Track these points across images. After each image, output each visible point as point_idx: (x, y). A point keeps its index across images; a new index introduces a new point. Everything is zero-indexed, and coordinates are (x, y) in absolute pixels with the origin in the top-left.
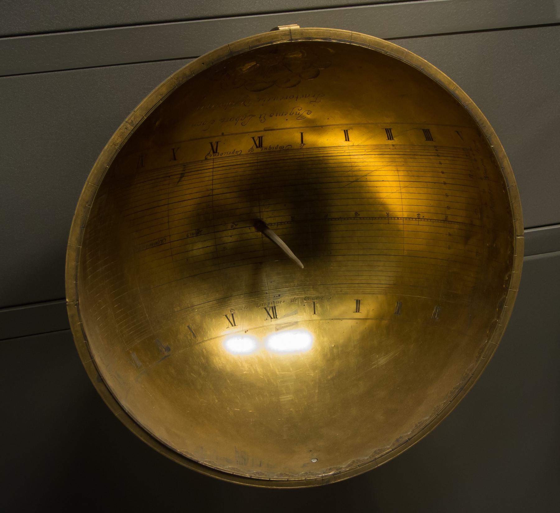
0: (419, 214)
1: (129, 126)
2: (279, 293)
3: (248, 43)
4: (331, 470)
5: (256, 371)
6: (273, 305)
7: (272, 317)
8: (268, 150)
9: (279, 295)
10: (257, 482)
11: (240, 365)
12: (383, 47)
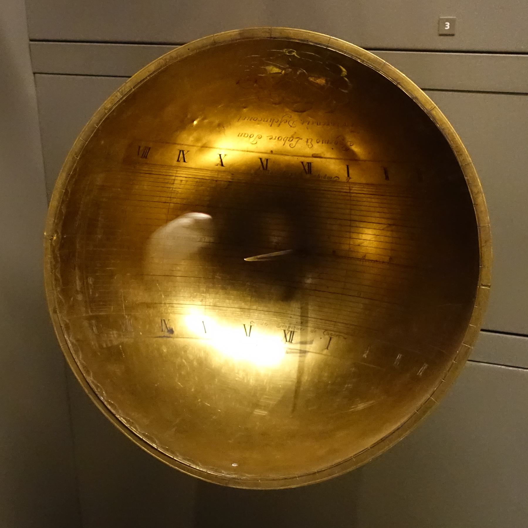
3: (231, 36)
5: (248, 381)
6: (293, 330)
7: (288, 340)
10: (163, 455)
12: (360, 56)
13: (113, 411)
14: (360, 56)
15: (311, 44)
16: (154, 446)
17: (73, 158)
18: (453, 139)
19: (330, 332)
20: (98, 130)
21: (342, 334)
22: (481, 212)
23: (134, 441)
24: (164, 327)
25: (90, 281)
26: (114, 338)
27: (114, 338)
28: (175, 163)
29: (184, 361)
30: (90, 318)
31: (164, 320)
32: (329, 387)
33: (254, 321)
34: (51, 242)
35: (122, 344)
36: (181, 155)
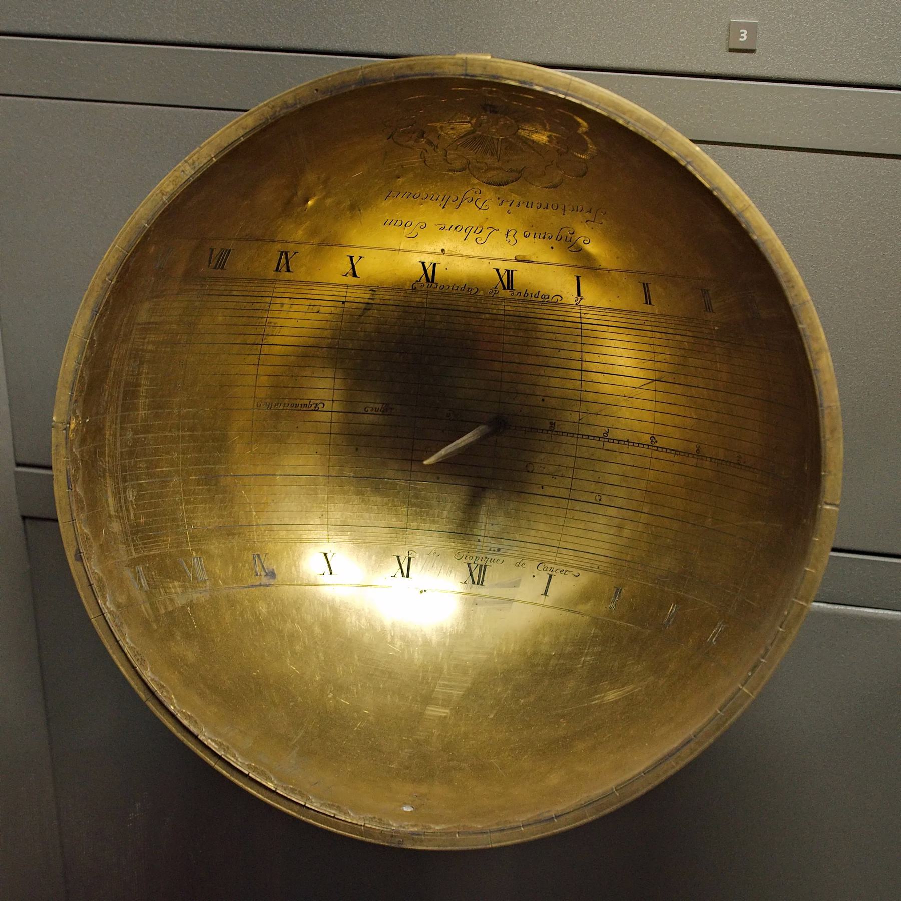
0: (740, 457)
1: (188, 168)
2: (500, 546)
4: (416, 826)
6: (483, 563)
8: (522, 297)
9: (499, 550)
10: (285, 801)
11: (389, 640)
12: (624, 113)
13: (192, 728)
14: (624, 113)
15: (538, 88)
16: (270, 786)
17: (104, 281)
18: (780, 260)
19: (549, 565)
20: (149, 230)
21: (570, 569)
22: (825, 383)
23: (232, 779)
24: (259, 568)
25: (131, 495)
26: (177, 595)
27: (177, 595)
28: (271, 274)
29: (297, 626)
30: (133, 563)
31: (258, 555)
32: (553, 662)
33: (415, 548)
34: (67, 434)
35: (191, 604)
36: (283, 260)
